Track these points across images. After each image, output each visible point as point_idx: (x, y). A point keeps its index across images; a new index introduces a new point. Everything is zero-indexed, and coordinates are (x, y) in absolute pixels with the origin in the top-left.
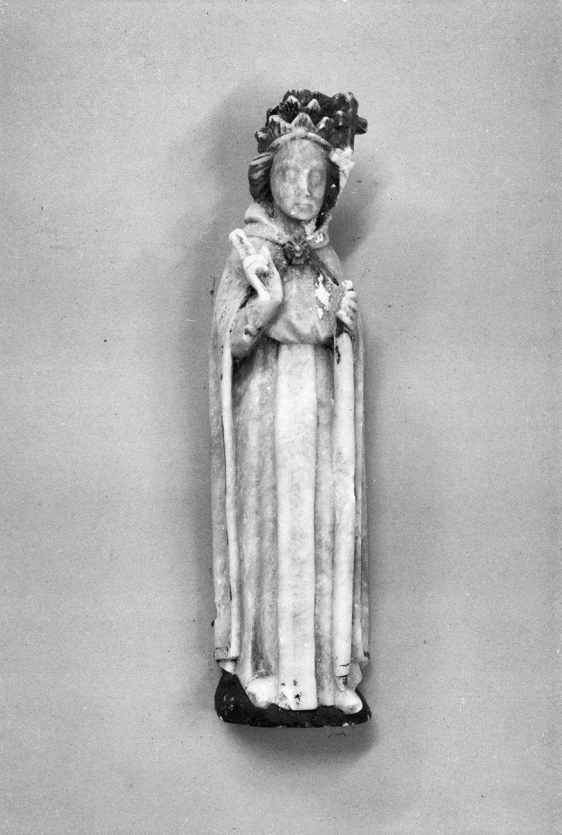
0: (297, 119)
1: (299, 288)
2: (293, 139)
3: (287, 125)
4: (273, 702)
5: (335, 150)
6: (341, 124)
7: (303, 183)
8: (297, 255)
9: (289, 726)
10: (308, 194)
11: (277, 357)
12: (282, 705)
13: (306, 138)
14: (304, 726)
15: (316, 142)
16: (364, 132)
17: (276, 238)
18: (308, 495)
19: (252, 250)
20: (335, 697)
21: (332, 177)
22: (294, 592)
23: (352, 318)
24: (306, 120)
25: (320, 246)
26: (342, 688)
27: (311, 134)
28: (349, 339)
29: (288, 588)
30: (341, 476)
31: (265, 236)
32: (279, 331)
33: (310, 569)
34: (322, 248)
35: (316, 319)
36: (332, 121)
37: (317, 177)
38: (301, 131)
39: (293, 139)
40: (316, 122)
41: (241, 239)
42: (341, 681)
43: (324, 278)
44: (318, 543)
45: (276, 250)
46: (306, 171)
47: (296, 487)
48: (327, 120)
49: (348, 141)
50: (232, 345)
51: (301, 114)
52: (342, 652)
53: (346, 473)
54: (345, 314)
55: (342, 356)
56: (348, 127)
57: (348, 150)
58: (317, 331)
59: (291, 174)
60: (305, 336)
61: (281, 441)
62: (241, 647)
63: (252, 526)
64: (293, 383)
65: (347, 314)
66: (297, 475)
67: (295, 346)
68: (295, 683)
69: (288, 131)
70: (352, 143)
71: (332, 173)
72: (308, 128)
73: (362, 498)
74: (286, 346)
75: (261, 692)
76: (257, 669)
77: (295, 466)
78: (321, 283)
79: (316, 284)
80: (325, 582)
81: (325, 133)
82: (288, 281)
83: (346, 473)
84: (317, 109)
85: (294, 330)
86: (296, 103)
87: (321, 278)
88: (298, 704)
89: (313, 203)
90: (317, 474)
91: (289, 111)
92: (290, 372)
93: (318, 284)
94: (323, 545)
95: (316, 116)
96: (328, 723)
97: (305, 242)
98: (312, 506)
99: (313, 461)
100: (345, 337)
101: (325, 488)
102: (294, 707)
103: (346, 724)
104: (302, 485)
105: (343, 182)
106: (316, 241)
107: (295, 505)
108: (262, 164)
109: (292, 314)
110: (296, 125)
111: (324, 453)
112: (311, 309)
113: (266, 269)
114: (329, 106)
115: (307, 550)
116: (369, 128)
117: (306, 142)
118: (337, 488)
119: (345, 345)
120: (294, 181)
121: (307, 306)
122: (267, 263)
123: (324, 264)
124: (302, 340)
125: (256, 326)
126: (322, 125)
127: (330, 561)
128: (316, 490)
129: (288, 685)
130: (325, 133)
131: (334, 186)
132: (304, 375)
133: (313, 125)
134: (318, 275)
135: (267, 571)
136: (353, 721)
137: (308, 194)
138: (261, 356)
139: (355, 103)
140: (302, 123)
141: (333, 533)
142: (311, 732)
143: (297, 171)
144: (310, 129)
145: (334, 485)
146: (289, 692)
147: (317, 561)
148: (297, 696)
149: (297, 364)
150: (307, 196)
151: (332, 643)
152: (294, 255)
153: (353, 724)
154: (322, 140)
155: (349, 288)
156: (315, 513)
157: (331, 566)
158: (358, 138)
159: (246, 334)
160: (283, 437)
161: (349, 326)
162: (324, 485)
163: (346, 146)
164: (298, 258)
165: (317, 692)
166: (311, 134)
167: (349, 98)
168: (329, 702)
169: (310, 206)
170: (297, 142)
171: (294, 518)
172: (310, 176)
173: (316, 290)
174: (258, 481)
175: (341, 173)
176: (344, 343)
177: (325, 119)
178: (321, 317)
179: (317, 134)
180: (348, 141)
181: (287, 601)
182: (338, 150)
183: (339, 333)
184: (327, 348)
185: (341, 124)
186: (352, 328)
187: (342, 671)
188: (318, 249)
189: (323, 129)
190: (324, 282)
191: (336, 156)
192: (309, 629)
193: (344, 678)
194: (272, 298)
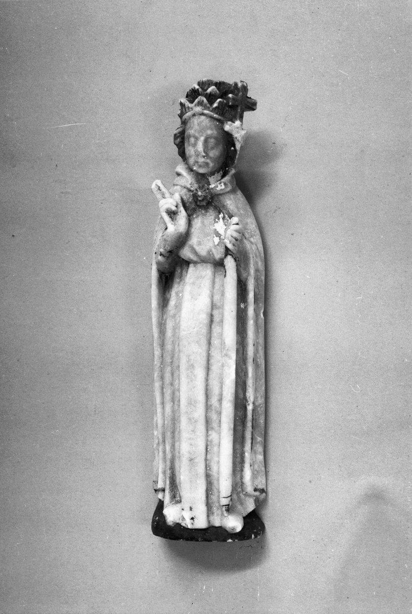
0: (196, 101)
1: (203, 223)
2: (194, 115)
3: (190, 105)
4: (178, 522)
5: (227, 123)
6: (230, 104)
7: (200, 147)
8: (200, 199)
9: (187, 539)
10: (204, 154)
11: (187, 272)
12: (183, 524)
13: (203, 114)
14: (198, 541)
15: (211, 117)
16: (254, 110)
17: (189, 186)
18: (200, 373)
19: (167, 195)
20: (221, 520)
21: (229, 141)
22: (191, 442)
23: (234, 245)
24: (203, 101)
25: (221, 192)
26: (225, 514)
27: (206, 112)
28: (232, 260)
29: (185, 440)
30: (226, 358)
31: (183, 185)
32: (186, 253)
33: (201, 427)
34: (223, 194)
35: (211, 245)
36: (225, 101)
37: (212, 141)
38: (198, 109)
39: (194, 115)
40: (211, 103)
41: (159, 189)
42: (224, 509)
43: (224, 215)
44: (208, 407)
45: (190, 195)
46: (202, 138)
47: (191, 367)
48: (220, 101)
49: (238, 116)
50: (157, 263)
51: (199, 97)
52: (224, 486)
53: (230, 358)
54: (229, 242)
55: (227, 272)
56: (237, 106)
57: (238, 123)
58: (213, 254)
59: (192, 140)
60: (205, 257)
61: (183, 333)
62: (165, 482)
63: (168, 394)
64: (197, 293)
65: (230, 242)
66: (192, 357)
67: (199, 265)
68: (191, 509)
69: (190, 110)
70: (241, 118)
71: (228, 140)
72: (205, 107)
73: (253, 375)
74: (192, 264)
75: (172, 514)
76: (175, 497)
77: (192, 350)
78: (221, 219)
79: (217, 220)
80: (213, 435)
81: (220, 110)
82: (196, 217)
83: (230, 358)
84: (215, 93)
85: (196, 253)
86: (198, 89)
87: (221, 215)
88: (192, 524)
89: (208, 161)
90: (209, 358)
91: (192, 95)
92: (193, 283)
93: (219, 219)
94: (213, 408)
95: (211, 98)
96: (216, 539)
97: (208, 189)
98: (203, 379)
99: (205, 347)
100: (229, 257)
101: (215, 368)
102: (190, 526)
103: (230, 540)
104: (195, 365)
105: (238, 146)
106: (217, 189)
107: (191, 379)
108: (179, 133)
109: (194, 241)
110: (195, 105)
111: (215, 342)
112: (209, 238)
113: (174, 208)
114: (224, 89)
115: (199, 412)
116: (259, 106)
117: (203, 117)
118: (224, 368)
119: (229, 264)
120: (195, 145)
121: (207, 235)
122: (175, 204)
123: (224, 205)
124: (203, 261)
125: (165, 250)
126: (215, 105)
127: (217, 421)
128: (208, 369)
129: (189, 512)
130: (220, 110)
131: (233, 148)
132: (202, 285)
133: (208, 105)
134: (220, 213)
135: (172, 430)
136: (236, 538)
137: (204, 154)
138: (179, 271)
139: (245, 89)
140: (200, 103)
141: (220, 400)
142: (200, 545)
143: (197, 139)
144: (206, 108)
145: (223, 366)
146: (187, 515)
147: (208, 421)
148: (192, 519)
149: (198, 278)
150: (204, 157)
151: (218, 480)
152: (197, 199)
153: (236, 540)
154: (215, 115)
155: (234, 222)
156: (207, 385)
157: (218, 425)
158: (247, 115)
159: (160, 256)
160: (184, 330)
161: (232, 251)
162: (215, 366)
163: (237, 120)
164: (200, 201)
165: (208, 516)
166: (206, 112)
167: (240, 85)
168: (217, 524)
169: (207, 164)
170: (197, 117)
171: (190, 387)
172: (206, 141)
173: (216, 224)
174: (172, 362)
175: (235, 140)
176: (230, 263)
177: (219, 100)
178: (216, 243)
179: (211, 111)
180: (238, 116)
181: (184, 448)
182: (229, 123)
183: (226, 256)
184: (219, 265)
185: (230, 104)
186: (235, 252)
187: (225, 502)
188: (220, 194)
189: (216, 107)
190: (224, 218)
191: (227, 127)
192: (201, 469)
193: (227, 507)
194: (175, 230)
